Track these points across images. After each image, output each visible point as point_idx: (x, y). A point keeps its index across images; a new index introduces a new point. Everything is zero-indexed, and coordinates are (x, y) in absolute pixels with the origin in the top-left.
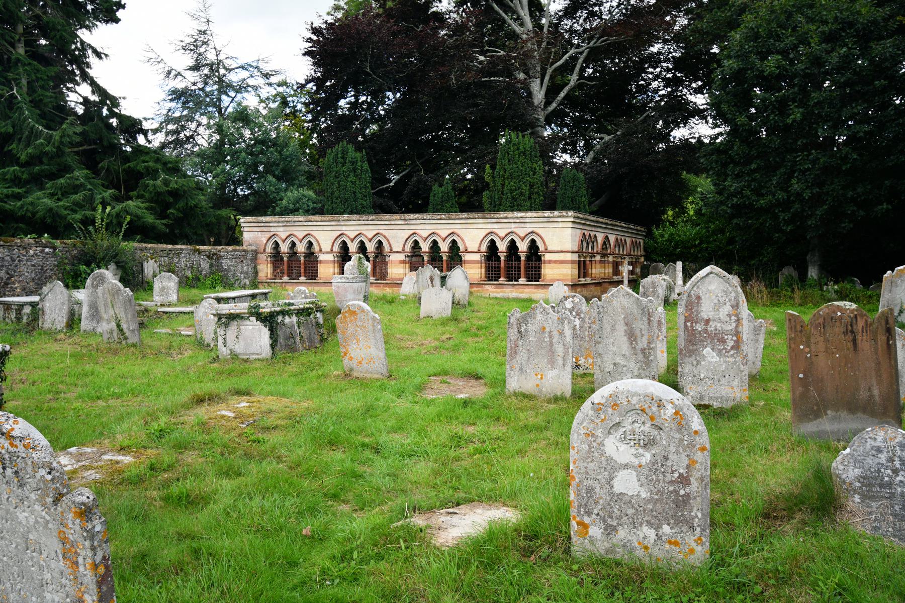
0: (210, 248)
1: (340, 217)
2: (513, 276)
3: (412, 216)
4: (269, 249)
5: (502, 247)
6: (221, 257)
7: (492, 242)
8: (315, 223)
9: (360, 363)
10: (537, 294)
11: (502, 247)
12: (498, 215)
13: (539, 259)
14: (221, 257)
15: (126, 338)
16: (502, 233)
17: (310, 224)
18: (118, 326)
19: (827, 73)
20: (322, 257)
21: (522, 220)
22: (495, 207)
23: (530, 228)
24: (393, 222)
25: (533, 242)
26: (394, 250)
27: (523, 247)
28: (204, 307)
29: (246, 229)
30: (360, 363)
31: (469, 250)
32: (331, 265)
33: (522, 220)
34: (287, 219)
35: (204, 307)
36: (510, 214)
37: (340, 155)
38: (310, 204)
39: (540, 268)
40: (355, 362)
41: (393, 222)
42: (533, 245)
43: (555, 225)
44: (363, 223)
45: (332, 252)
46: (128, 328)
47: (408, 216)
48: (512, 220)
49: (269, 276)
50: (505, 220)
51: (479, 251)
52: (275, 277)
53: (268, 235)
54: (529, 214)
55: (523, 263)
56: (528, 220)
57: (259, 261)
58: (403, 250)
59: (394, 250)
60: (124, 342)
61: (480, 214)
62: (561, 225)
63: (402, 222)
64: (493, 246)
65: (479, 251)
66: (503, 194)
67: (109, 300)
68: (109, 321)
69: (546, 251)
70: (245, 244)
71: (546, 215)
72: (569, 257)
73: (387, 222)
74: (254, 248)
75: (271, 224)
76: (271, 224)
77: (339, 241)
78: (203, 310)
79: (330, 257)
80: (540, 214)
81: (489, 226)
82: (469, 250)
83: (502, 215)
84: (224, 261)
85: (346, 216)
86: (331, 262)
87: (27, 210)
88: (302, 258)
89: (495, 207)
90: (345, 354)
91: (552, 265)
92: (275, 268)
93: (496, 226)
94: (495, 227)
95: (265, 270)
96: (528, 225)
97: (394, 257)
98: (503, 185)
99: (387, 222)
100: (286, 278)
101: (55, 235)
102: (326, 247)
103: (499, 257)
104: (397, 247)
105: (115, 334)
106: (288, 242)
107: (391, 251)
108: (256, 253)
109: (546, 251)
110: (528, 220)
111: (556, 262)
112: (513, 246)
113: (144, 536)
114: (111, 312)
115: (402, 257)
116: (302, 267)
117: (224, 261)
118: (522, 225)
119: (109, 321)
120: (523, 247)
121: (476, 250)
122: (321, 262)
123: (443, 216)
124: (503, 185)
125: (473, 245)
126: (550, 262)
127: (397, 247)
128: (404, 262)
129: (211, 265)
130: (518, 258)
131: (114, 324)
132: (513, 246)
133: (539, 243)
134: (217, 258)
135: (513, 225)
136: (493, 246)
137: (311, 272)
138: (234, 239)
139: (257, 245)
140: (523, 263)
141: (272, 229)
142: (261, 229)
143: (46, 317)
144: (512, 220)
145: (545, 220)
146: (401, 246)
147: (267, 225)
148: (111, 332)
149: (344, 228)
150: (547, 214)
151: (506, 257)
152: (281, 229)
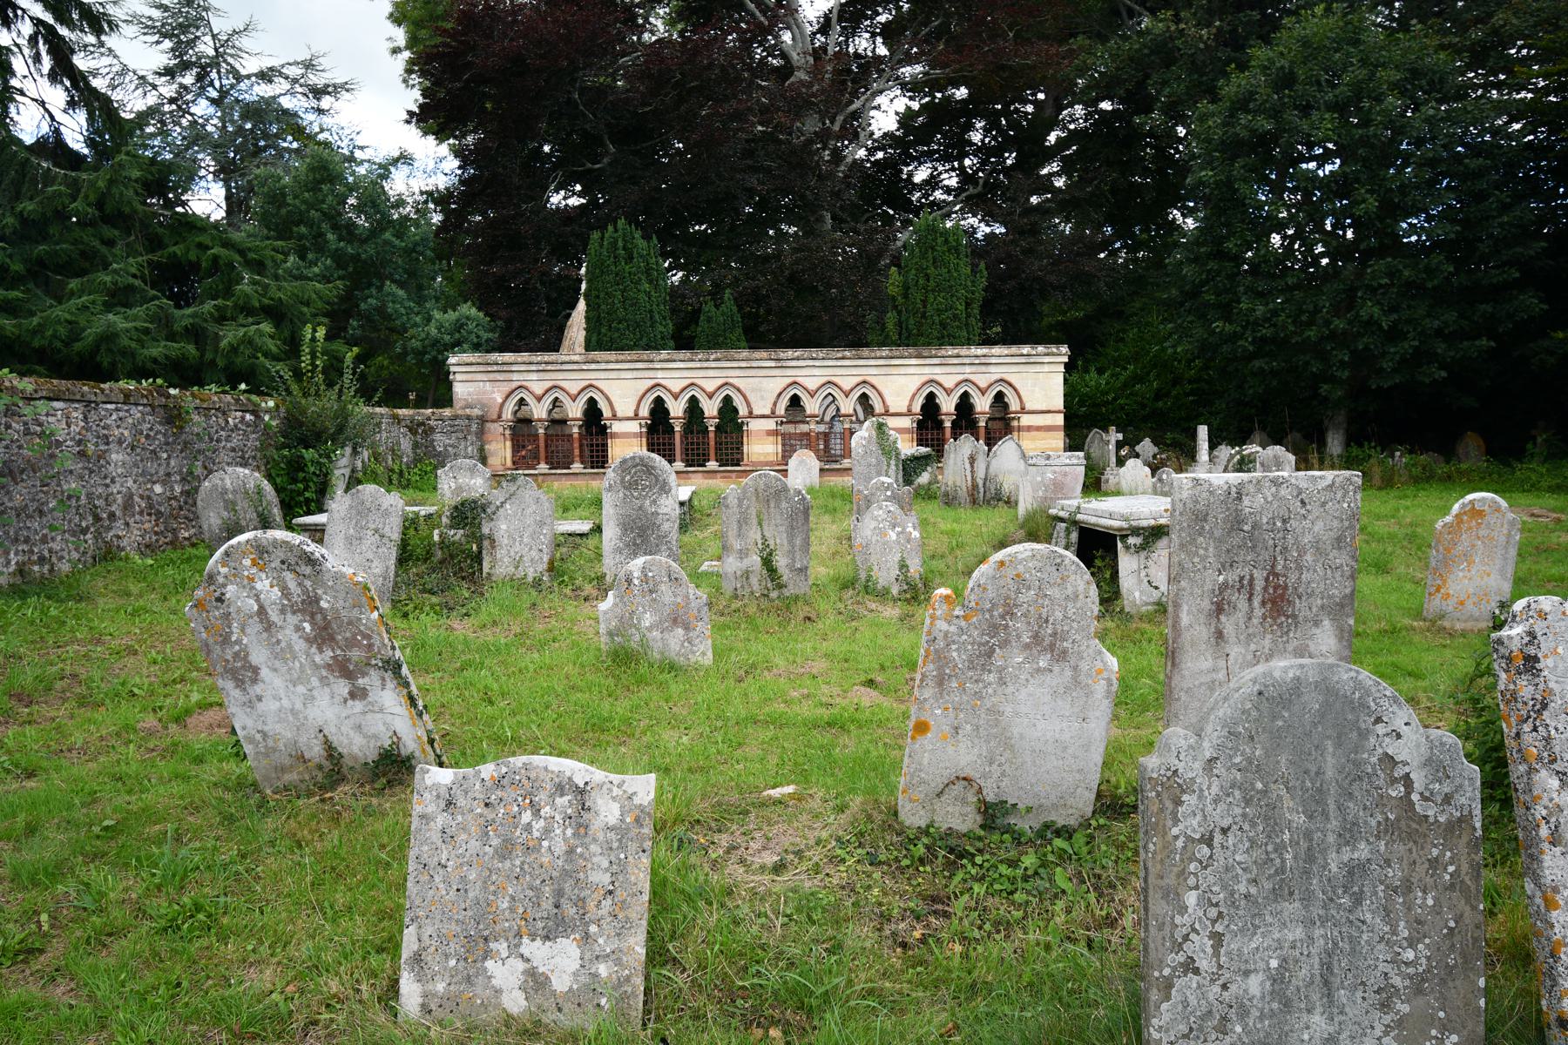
0: (411, 412)
1: (653, 354)
2: (559, 461)
3: (790, 353)
4: (508, 414)
5: (677, 409)
6: (432, 430)
7: (659, 402)
8: (603, 366)
9: (1462, 603)
10: (730, 487)
11: (677, 409)
12: (943, 352)
13: (603, 430)
14: (432, 430)
15: (780, 586)
16: (949, 382)
17: (593, 366)
18: (767, 563)
19: (555, 167)
20: (616, 427)
21: (983, 360)
22: (908, 338)
23: (996, 372)
24: (755, 364)
25: (727, 400)
26: (756, 412)
27: (710, 408)
28: (875, 518)
29: (458, 377)
30: (1462, 603)
31: (892, 410)
32: (636, 441)
33: (983, 360)
34: (546, 358)
35: (875, 518)
36: (964, 351)
37: (620, 244)
38: (481, 333)
39: (605, 445)
40: (1452, 602)
41: (755, 364)
42: (728, 408)
43: (1038, 368)
44: (698, 365)
45: (636, 416)
46: (1013, 560)
47: (782, 354)
48: (967, 361)
49: (509, 463)
50: (956, 361)
51: (909, 413)
52: (517, 464)
53: (507, 388)
54: (996, 350)
55: (712, 435)
56: (993, 360)
57: (488, 437)
58: (773, 412)
59: (756, 412)
60: (774, 595)
61: (911, 350)
62: (1046, 368)
63: (773, 364)
64: (659, 409)
65: (909, 413)
66: (924, 316)
67: (753, 511)
68: (743, 554)
69: (1023, 410)
70: (458, 404)
71: (1025, 351)
72: (1026, 420)
73: (743, 364)
74: (477, 412)
75: (514, 368)
76: (514, 368)
77: (651, 397)
78: (873, 524)
79: (634, 427)
80: (1014, 349)
81: (927, 370)
82: (892, 410)
83: (951, 351)
84: (437, 437)
85: (664, 354)
86: (635, 435)
87: (54, 336)
88: (541, 431)
89: (908, 338)
90: (1438, 590)
91: (1034, 433)
92: (516, 448)
93: (937, 370)
94: (937, 373)
95: (501, 453)
96: (992, 369)
97: (755, 425)
98: (924, 302)
99: (743, 364)
100: (543, 467)
101: (255, 390)
102: (625, 407)
103: (942, 422)
104: (762, 408)
105: (754, 580)
106: (548, 400)
107: (751, 415)
108: (483, 420)
109: (1023, 410)
110: (993, 360)
111: (1039, 429)
112: (694, 407)
113: (468, 1030)
114: (754, 534)
115: (770, 424)
116: (576, 445)
117: (437, 437)
118: (983, 368)
119: (743, 554)
120: (710, 408)
121: (904, 410)
122: (614, 435)
123: (848, 354)
124: (924, 302)
125: (898, 403)
126: (1029, 429)
127: (762, 408)
128: (775, 433)
129: (416, 446)
130: (671, 429)
131: (755, 560)
132: (694, 407)
133: (738, 402)
134: (424, 432)
135: (968, 369)
136: (659, 409)
137: (731, 455)
138: (439, 391)
139: (483, 406)
140: (677, 437)
141: (515, 377)
142: (492, 376)
143: (501, 553)
144: (967, 361)
145: (1023, 360)
146: (770, 406)
147: (505, 369)
148: (747, 574)
149: (660, 374)
150: (1026, 349)
151: (953, 422)
152: (534, 376)
